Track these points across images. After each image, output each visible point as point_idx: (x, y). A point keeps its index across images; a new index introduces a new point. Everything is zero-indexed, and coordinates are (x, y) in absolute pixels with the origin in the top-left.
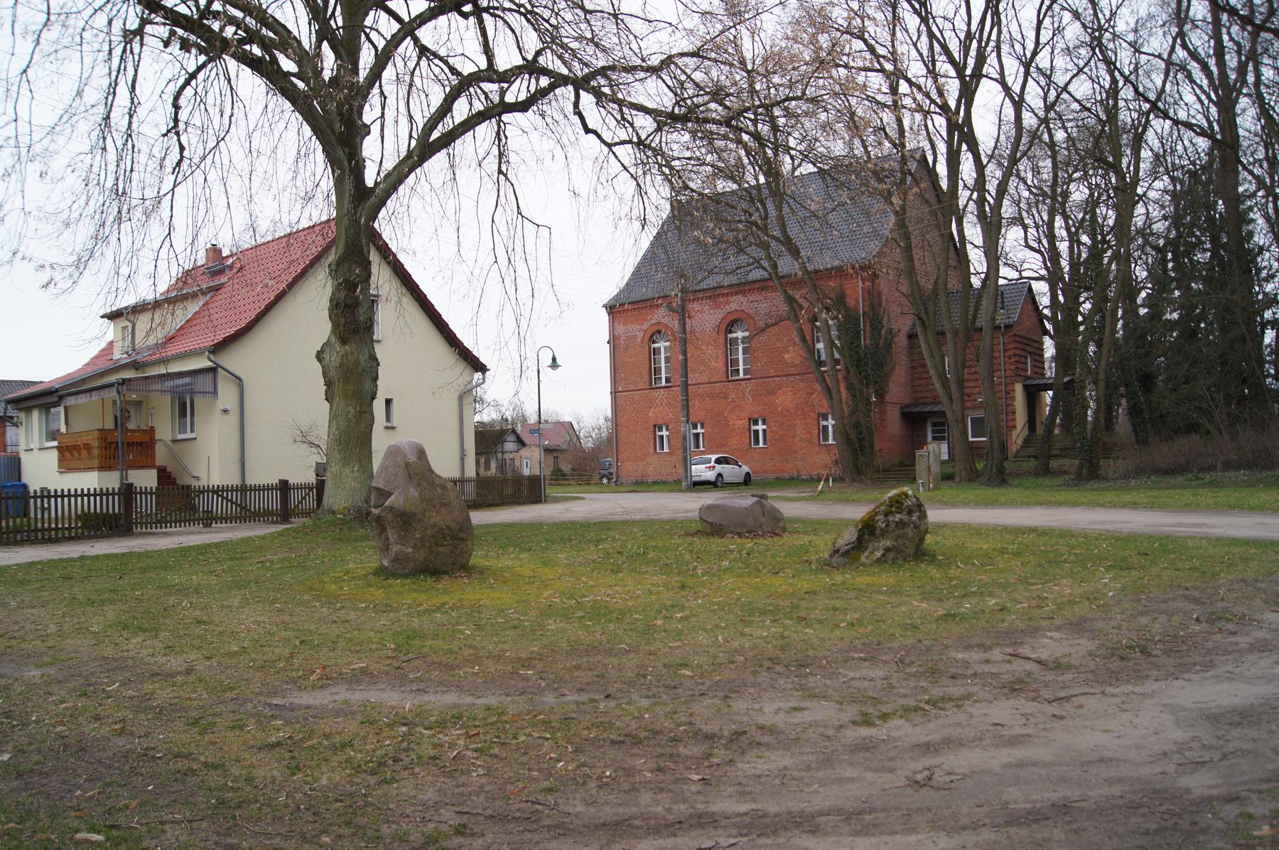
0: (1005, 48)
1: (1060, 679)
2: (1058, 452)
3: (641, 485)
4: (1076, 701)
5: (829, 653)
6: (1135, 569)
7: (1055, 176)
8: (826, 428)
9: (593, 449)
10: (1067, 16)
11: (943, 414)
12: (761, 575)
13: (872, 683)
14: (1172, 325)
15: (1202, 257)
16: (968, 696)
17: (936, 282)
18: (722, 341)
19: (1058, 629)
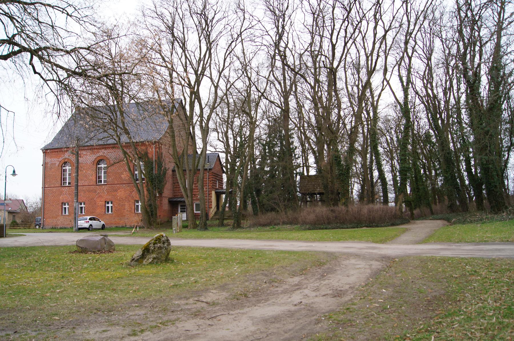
0: (213, 66)
1: (214, 309)
2: (227, 218)
3: (54, 229)
4: (218, 318)
5: (123, 305)
6: (246, 263)
7: (229, 115)
8: (138, 206)
9: (33, 212)
10: (235, 58)
11: (184, 202)
12: (100, 270)
13: (139, 317)
14: (267, 172)
15: (277, 149)
16: (177, 319)
17: (183, 151)
18: (94, 169)
19: (215, 289)
